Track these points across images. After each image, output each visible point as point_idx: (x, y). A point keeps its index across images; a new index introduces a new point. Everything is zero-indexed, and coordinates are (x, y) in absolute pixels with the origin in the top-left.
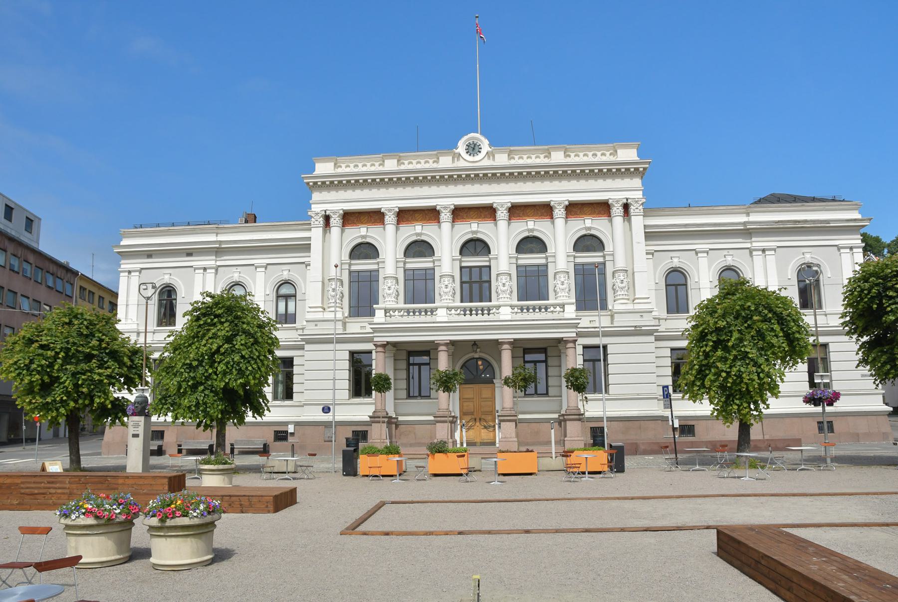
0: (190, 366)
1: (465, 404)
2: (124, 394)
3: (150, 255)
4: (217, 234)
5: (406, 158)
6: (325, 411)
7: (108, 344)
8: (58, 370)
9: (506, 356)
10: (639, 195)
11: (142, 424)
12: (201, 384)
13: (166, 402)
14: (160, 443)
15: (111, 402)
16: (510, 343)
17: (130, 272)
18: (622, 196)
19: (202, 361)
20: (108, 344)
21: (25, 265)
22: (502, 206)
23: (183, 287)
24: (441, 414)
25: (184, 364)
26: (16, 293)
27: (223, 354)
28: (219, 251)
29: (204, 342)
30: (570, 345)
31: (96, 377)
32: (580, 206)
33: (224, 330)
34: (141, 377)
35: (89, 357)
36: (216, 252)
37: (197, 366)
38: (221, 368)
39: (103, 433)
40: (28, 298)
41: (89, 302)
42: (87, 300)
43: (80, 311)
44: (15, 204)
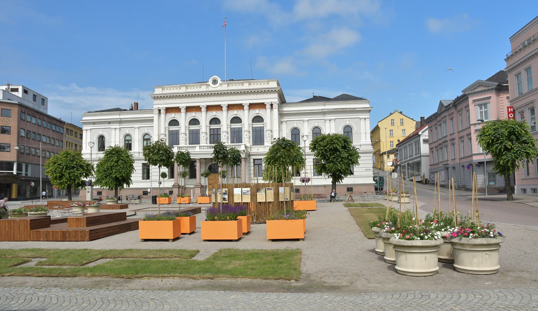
0: (105, 171)
1: (210, 181)
2: (85, 179)
3: (94, 123)
4: (120, 115)
5: (189, 86)
7: (79, 163)
8: (64, 172)
11: (90, 188)
12: (108, 176)
13: (98, 182)
14: (100, 196)
15: (81, 182)
16: (199, 160)
17: (87, 130)
18: (270, 101)
19: (109, 168)
20: (79, 163)
21: (44, 122)
22: (224, 105)
23: (107, 136)
24: (197, 185)
25: (103, 170)
26: (40, 135)
27: (115, 167)
28: (120, 122)
29: (109, 163)
31: (76, 174)
33: (115, 159)
34: (90, 173)
35: (73, 167)
36: (120, 122)
37: (107, 171)
38: (114, 171)
39: (79, 194)
40: (45, 136)
42: (70, 134)
43: (70, 152)
44: (37, 93)
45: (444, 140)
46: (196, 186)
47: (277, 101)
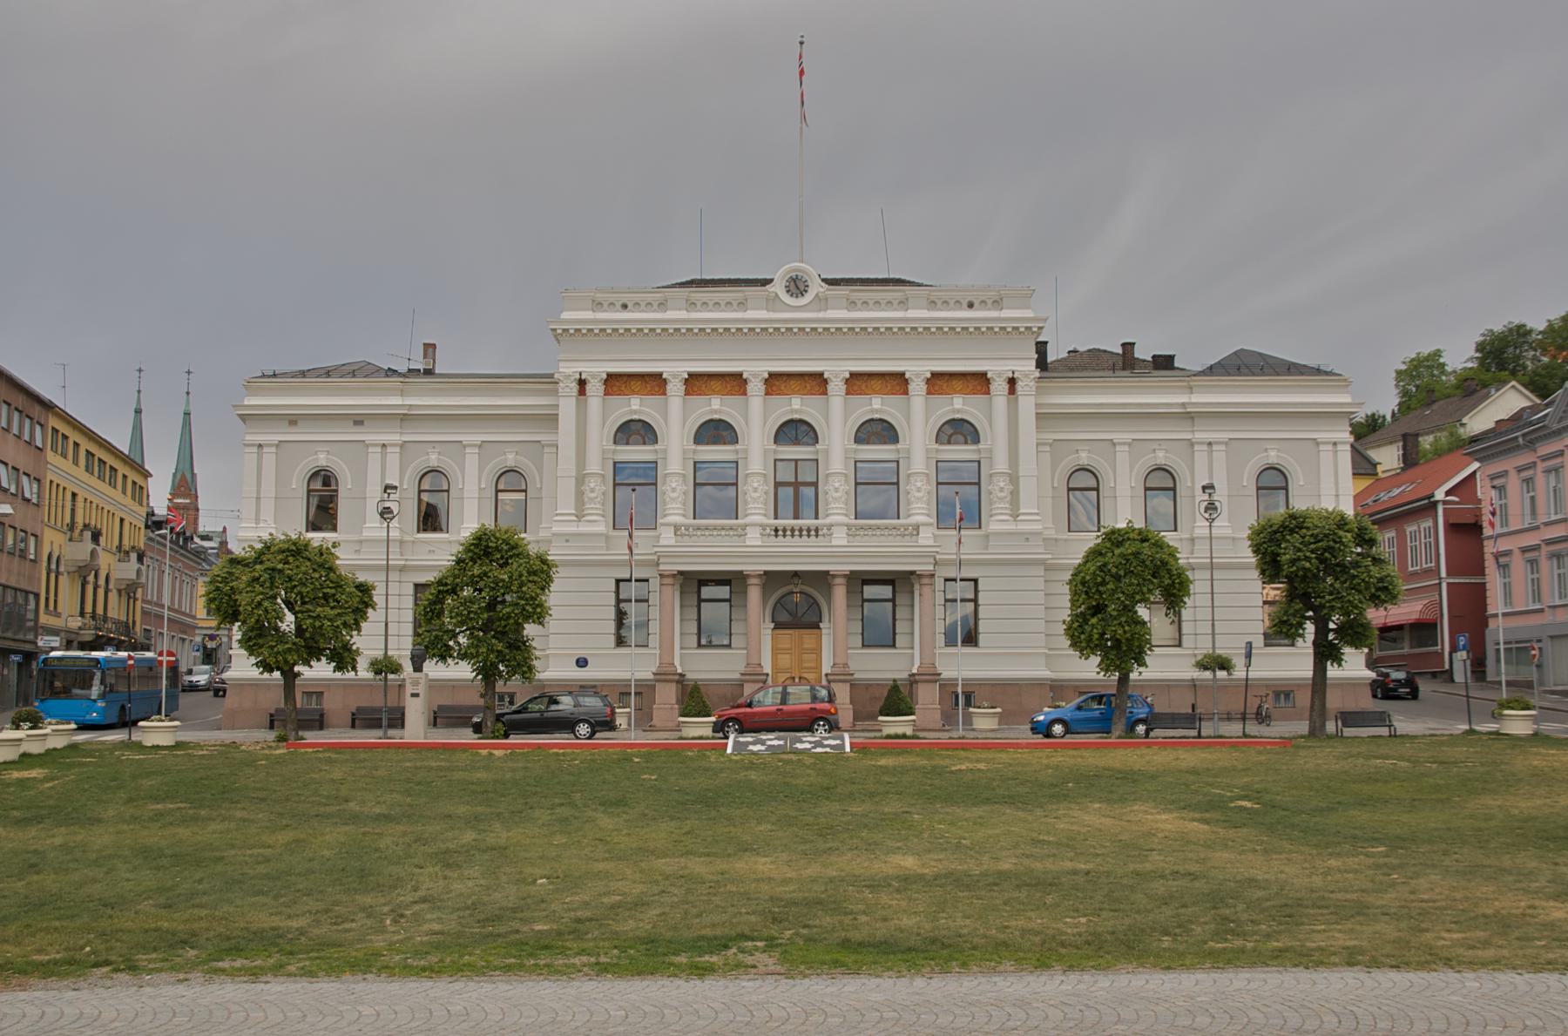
3: (293, 421)
6: (581, 664)
10: (937, 651)
28: (405, 418)
30: (925, 581)
32: (946, 378)
36: (402, 420)
41: (99, 478)
46: (418, 668)
47: (1034, 368)
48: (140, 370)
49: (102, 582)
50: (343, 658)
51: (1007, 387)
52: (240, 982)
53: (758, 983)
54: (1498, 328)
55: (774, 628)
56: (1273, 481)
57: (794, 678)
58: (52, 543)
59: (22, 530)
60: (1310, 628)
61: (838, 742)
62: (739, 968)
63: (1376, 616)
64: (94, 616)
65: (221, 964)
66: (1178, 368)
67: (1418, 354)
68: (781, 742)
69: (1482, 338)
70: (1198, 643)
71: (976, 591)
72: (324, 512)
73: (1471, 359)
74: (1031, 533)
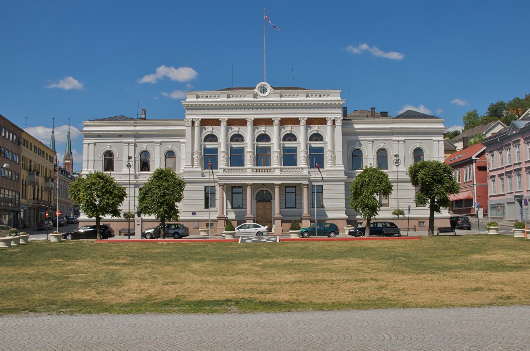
3: (99, 136)
9: (277, 190)
17: (89, 144)
18: (332, 116)
45: (517, 167)
46: (139, 216)
47: (341, 116)
48: (53, 119)
49: (40, 188)
50: (116, 213)
51: (332, 122)
52: (67, 315)
53: (229, 315)
54: (495, 103)
55: (257, 202)
56: (418, 153)
57: (263, 218)
58: (23, 176)
59: (14, 172)
60: (429, 201)
61: (275, 239)
62: (226, 311)
63: (452, 197)
64: (38, 200)
65: (63, 310)
66: (389, 116)
67: (470, 111)
68: (257, 239)
69: (490, 106)
70: (393, 206)
71: (322, 190)
72: (109, 165)
73: (487, 113)
74: (340, 171)
